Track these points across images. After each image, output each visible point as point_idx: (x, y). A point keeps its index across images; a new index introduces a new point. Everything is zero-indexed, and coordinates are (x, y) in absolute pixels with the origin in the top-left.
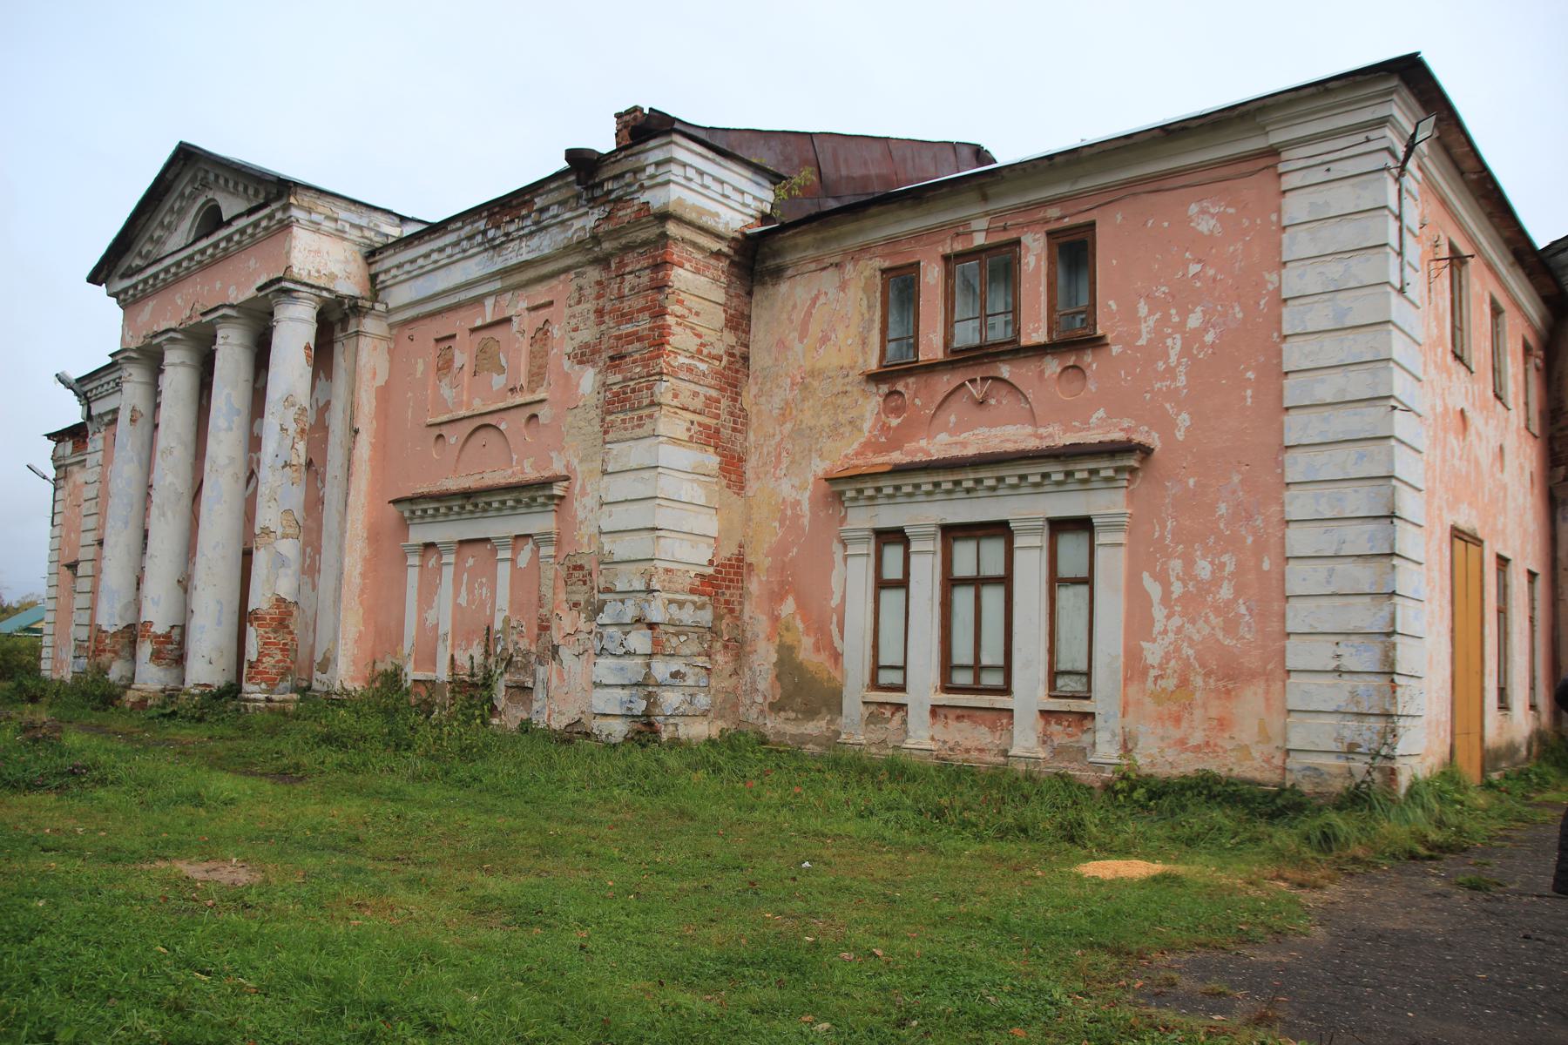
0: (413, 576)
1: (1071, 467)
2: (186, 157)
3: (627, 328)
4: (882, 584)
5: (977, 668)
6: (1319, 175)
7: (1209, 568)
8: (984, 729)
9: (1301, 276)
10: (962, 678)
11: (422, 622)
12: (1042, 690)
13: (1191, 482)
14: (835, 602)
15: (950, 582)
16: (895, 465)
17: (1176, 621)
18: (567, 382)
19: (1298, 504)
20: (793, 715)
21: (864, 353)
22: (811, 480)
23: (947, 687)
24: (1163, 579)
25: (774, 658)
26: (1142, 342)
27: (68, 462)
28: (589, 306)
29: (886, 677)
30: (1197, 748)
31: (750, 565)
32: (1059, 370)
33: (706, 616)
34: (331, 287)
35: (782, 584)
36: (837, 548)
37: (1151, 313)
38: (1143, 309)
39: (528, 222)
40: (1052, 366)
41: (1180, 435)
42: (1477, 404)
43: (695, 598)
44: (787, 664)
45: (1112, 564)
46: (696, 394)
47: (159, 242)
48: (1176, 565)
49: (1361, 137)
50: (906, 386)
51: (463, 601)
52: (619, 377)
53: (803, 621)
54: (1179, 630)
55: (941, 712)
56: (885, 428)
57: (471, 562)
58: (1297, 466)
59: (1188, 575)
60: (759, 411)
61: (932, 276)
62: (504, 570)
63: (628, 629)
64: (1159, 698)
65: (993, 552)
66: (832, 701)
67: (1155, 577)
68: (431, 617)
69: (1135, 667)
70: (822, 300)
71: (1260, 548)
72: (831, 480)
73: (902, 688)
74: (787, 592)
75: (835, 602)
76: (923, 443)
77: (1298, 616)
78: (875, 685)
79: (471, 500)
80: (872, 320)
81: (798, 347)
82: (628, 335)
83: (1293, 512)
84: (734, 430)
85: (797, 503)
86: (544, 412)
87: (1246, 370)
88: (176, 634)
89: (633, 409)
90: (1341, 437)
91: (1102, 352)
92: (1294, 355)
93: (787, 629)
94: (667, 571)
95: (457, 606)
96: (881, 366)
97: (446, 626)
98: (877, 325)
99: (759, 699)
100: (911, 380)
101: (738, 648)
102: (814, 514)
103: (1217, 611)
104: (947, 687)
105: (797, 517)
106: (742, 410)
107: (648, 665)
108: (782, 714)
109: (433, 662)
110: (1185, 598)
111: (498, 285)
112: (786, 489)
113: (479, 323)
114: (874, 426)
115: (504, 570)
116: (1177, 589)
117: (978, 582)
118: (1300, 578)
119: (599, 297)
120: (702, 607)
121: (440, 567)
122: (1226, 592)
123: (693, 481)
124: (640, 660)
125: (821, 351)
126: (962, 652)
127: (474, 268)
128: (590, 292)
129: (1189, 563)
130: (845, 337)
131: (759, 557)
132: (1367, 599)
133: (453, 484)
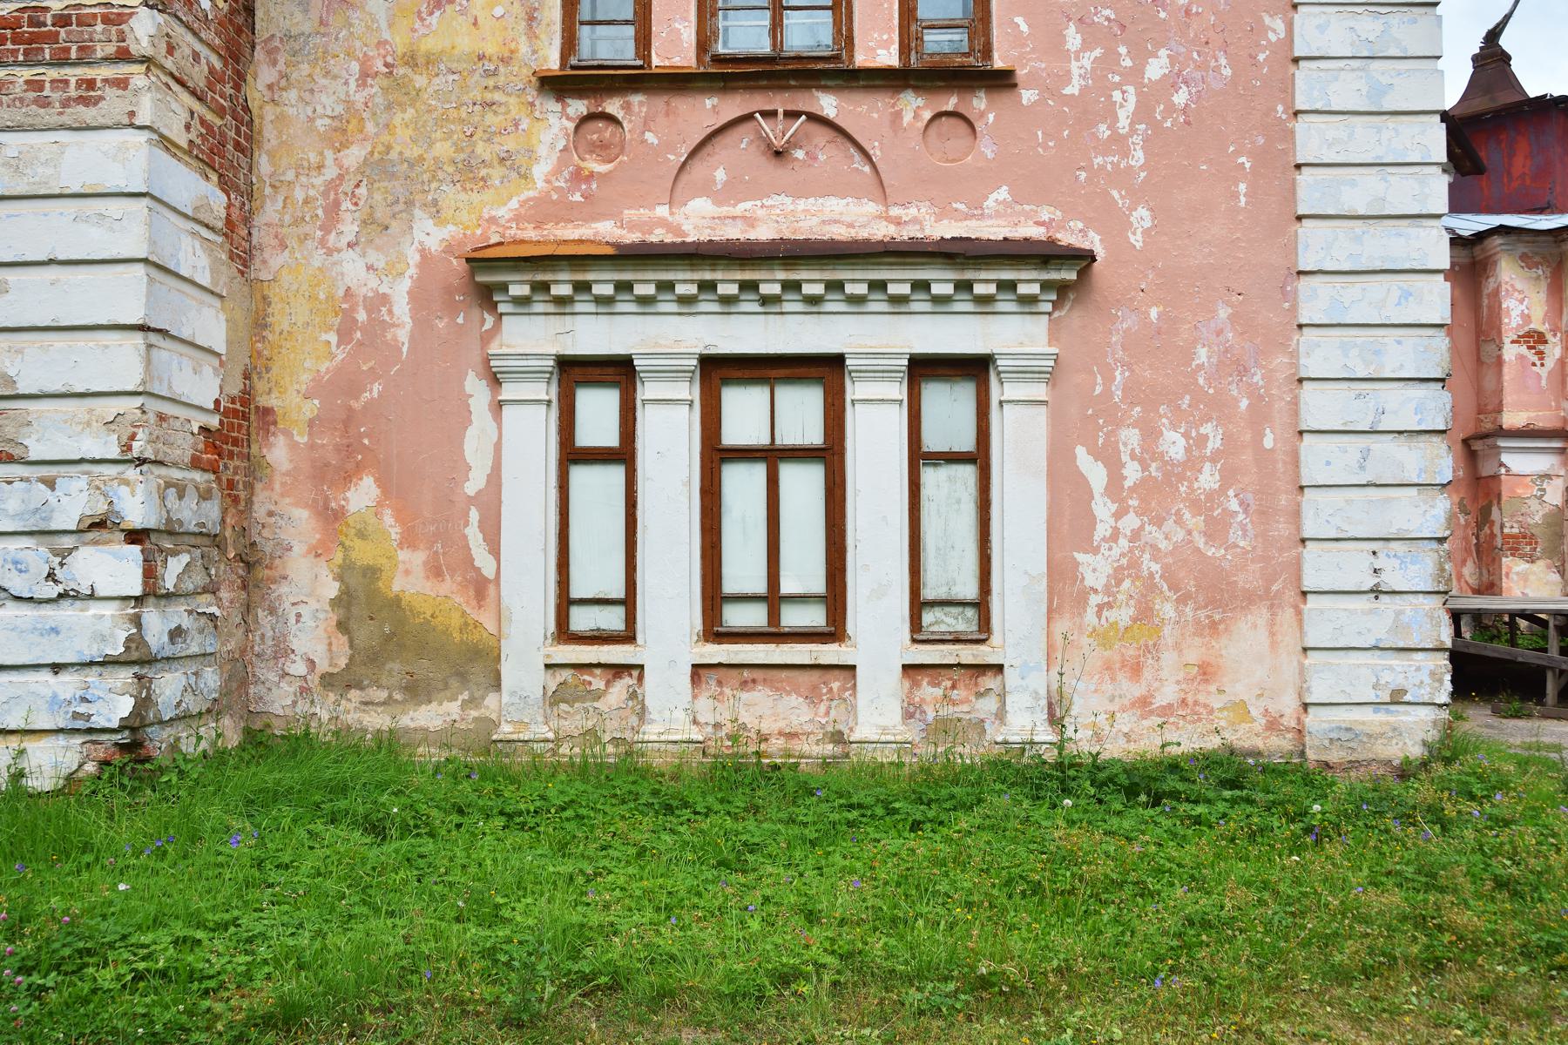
1: (968, 275)
4: (572, 455)
5: (773, 599)
7: (1182, 442)
8: (794, 700)
9: (1321, 28)
10: (752, 617)
13: (1154, 313)
14: (474, 484)
17: (1130, 522)
21: (532, 35)
23: (714, 631)
25: (332, 589)
26: (1073, 89)
29: (582, 619)
30: (1167, 710)
31: (267, 412)
32: (927, 115)
35: (348, 450)
36: (477, 391)
37: (1087, 46)
38: (1073, 39)
40: (913, 107)
41: (1137, 240)
48: (1130, 437)
50: (627, 107)
53: (399, 519)
54: (1136, 535)
55: (711, 678)
56: (579, 177)
59: (1149, 452)
60: (281, 119)
63: (67, 542)
64: (1103, 638)
67: (1097, 454)
71: (1259, 417)
74: (359, 469)
75: (474, 484)
77: (1319, 514)
78: (564, 633)
83: (1311, 366)
85: (384, 299)
87: (1238, 153)
89: (61, 61)
90: (1378, 265)
91: (1004, 98)
92: (1311, 139)
93: (361, 535)
94: (162, 418)
96: (563, 64)
99: (299, 668)
100: (636, 99)
102: (421, 324)
103: (1196, 506)
104: (564, 633)
105: (379, 326)
107: (137, 621)
108: (354, 694)
110: (1140, 487)
114: (557, 172)
116: (1132, 472)
117: (772, 456)
118: (1319, 459)
122: (1208, 479)
123: (194, 234)
124: (110, 609)
125: (434, 20)
129: (1151, 434)
132: (1413, 491)
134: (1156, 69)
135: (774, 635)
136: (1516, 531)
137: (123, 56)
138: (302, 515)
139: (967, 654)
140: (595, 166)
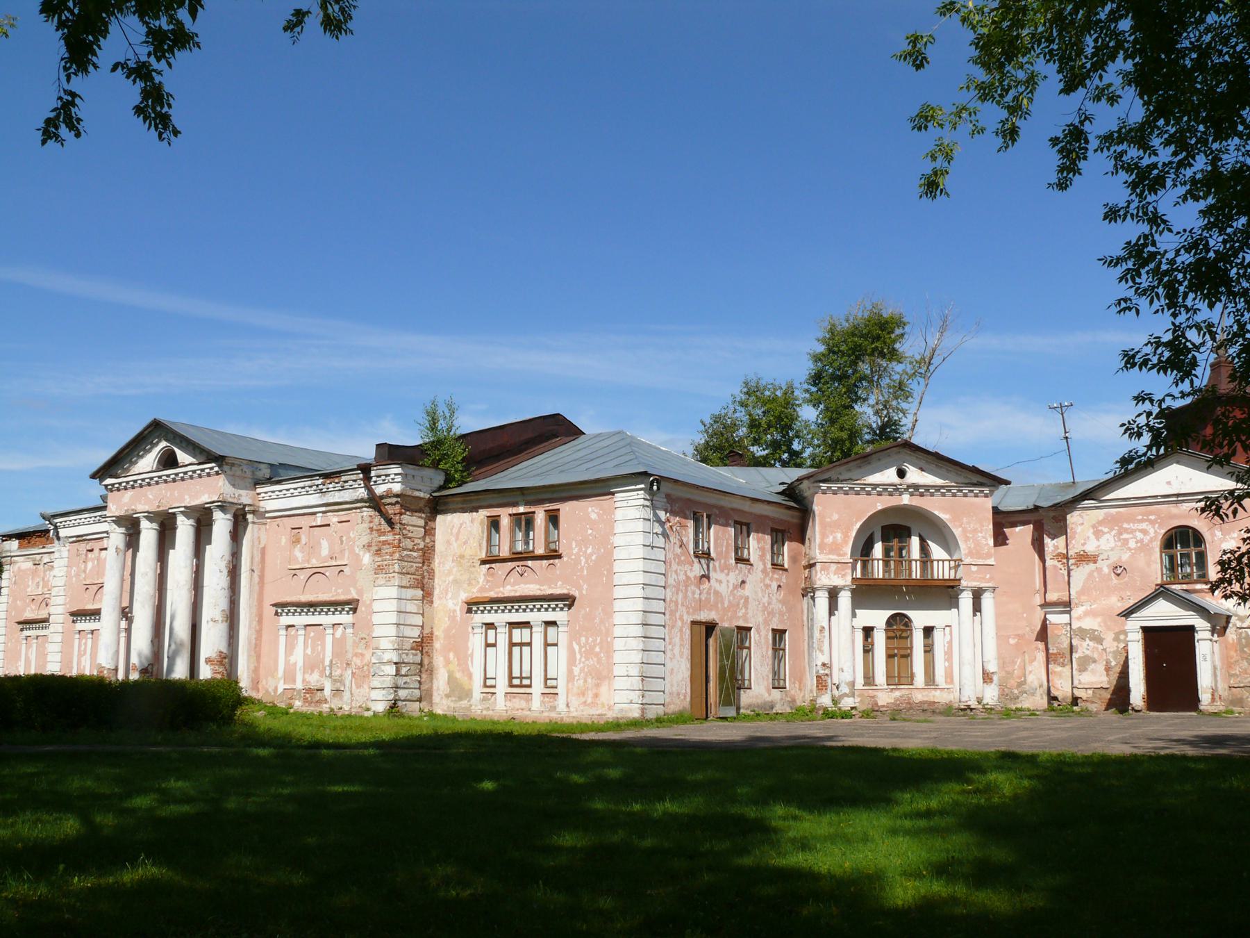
0: (282, 640)
2: (156, 429)
3: (383, 538)
4: (488, 645)
6: (624, 504)
10: (516, 682)
11: (287, 662)
12: (542, 685)
15: (512, 644)
16: (491, 598)
18: (358, 559)
19: (618, 619)
20: (454, 699)
22: (460, 601)
23: (546, 686)
24: (579, 644)
27: (12, 554)
28: (366, 525)
29: (489, 682)
30: (589, 704)
33: (418, 659)
34: (240, 502)
39: (339, 485)
40: (545, 563)
41: (584, 592)
42: (718, 569)
43: (414, 652)
44: (451, 680)
45: (563, 639)
46: (412, 566)
47: (128, 470)
48: (583, 639)
49: (635, 493)
51: (309, 651)
52: (380, 559)
56: (488, 581)
57: (312, 634)
58: (617, 605)
61: (505, 522)
62: (329, 639)
65: (526, 631)
66: (468, 694)
68: (292, 659)
69: (570, 677)
70: (464, 525)
72: (468, 604)
73: (494, 687)
75: (470, 652)
76: (501, 589)
77: (617, 657)
78: (485, 686)
79: (312, 606)
80: (483, 537)
81: (455, 544)
82: (383, 541)
84: (429, 579)
85: (455, 611)
86: (346, 569)
88: (150, 667)
92: (617, 567)
95: (305, 655)
96: (487, 556)
97: (300, 664)
98: (485, 539)
101: (431, 671)
104: (512, 686)
105: (455, 617)
106: (432, 569)
109: (294, 681)
111: (323, 509)
112: (450, 604)
113: (314, 524)
115: (329, 639)
117: (521, 645)
118: (618, 644)
119: (371, 522)
120: (416, 655)
121: (296, 637)
122: (597, 649)
126: (516, 673)
127: (314, 499)
128: (368, 519)
130: (474, 543)
131: (438, 633)
133: (304, 598)
134: (589, 551)
135: (521, 686)
136: (1055, 651)
137: (394, 572)
138: (442, 658)
139: (552, 691)
140: (490, 579)
